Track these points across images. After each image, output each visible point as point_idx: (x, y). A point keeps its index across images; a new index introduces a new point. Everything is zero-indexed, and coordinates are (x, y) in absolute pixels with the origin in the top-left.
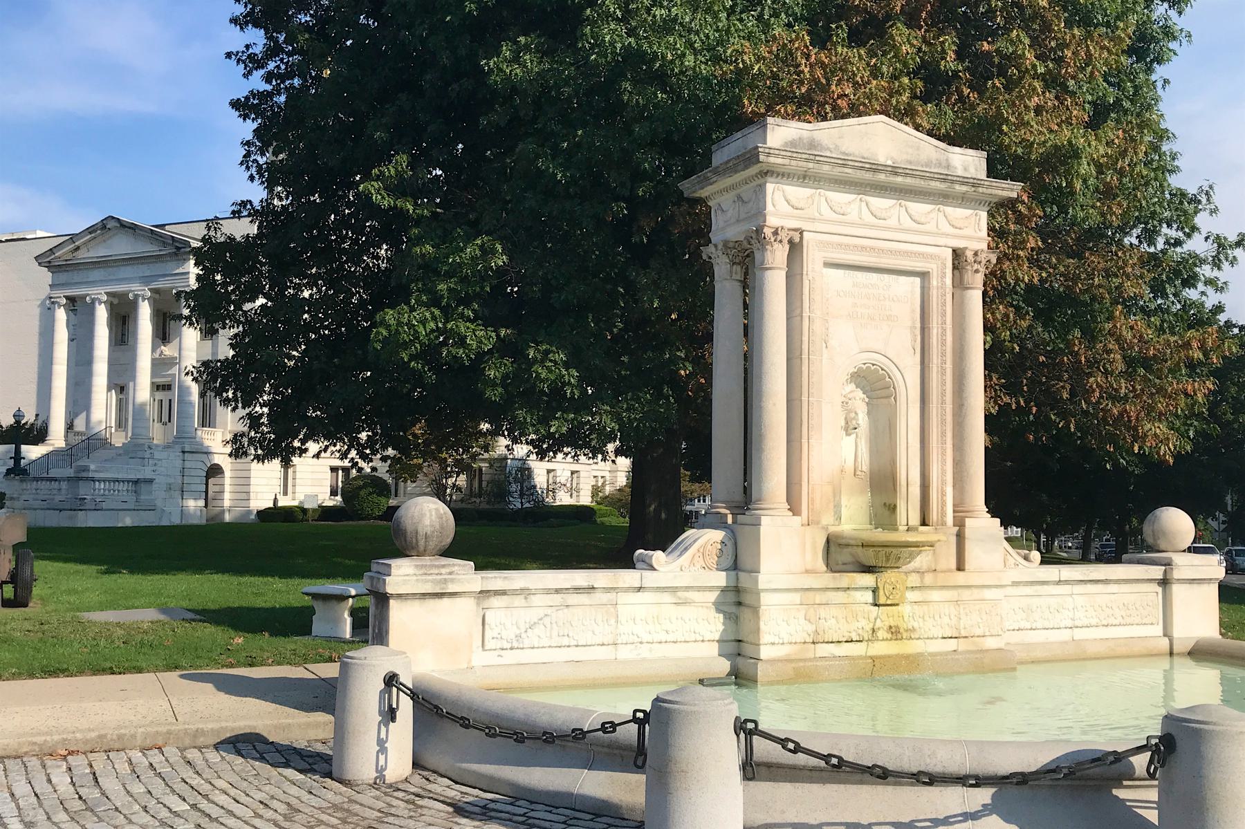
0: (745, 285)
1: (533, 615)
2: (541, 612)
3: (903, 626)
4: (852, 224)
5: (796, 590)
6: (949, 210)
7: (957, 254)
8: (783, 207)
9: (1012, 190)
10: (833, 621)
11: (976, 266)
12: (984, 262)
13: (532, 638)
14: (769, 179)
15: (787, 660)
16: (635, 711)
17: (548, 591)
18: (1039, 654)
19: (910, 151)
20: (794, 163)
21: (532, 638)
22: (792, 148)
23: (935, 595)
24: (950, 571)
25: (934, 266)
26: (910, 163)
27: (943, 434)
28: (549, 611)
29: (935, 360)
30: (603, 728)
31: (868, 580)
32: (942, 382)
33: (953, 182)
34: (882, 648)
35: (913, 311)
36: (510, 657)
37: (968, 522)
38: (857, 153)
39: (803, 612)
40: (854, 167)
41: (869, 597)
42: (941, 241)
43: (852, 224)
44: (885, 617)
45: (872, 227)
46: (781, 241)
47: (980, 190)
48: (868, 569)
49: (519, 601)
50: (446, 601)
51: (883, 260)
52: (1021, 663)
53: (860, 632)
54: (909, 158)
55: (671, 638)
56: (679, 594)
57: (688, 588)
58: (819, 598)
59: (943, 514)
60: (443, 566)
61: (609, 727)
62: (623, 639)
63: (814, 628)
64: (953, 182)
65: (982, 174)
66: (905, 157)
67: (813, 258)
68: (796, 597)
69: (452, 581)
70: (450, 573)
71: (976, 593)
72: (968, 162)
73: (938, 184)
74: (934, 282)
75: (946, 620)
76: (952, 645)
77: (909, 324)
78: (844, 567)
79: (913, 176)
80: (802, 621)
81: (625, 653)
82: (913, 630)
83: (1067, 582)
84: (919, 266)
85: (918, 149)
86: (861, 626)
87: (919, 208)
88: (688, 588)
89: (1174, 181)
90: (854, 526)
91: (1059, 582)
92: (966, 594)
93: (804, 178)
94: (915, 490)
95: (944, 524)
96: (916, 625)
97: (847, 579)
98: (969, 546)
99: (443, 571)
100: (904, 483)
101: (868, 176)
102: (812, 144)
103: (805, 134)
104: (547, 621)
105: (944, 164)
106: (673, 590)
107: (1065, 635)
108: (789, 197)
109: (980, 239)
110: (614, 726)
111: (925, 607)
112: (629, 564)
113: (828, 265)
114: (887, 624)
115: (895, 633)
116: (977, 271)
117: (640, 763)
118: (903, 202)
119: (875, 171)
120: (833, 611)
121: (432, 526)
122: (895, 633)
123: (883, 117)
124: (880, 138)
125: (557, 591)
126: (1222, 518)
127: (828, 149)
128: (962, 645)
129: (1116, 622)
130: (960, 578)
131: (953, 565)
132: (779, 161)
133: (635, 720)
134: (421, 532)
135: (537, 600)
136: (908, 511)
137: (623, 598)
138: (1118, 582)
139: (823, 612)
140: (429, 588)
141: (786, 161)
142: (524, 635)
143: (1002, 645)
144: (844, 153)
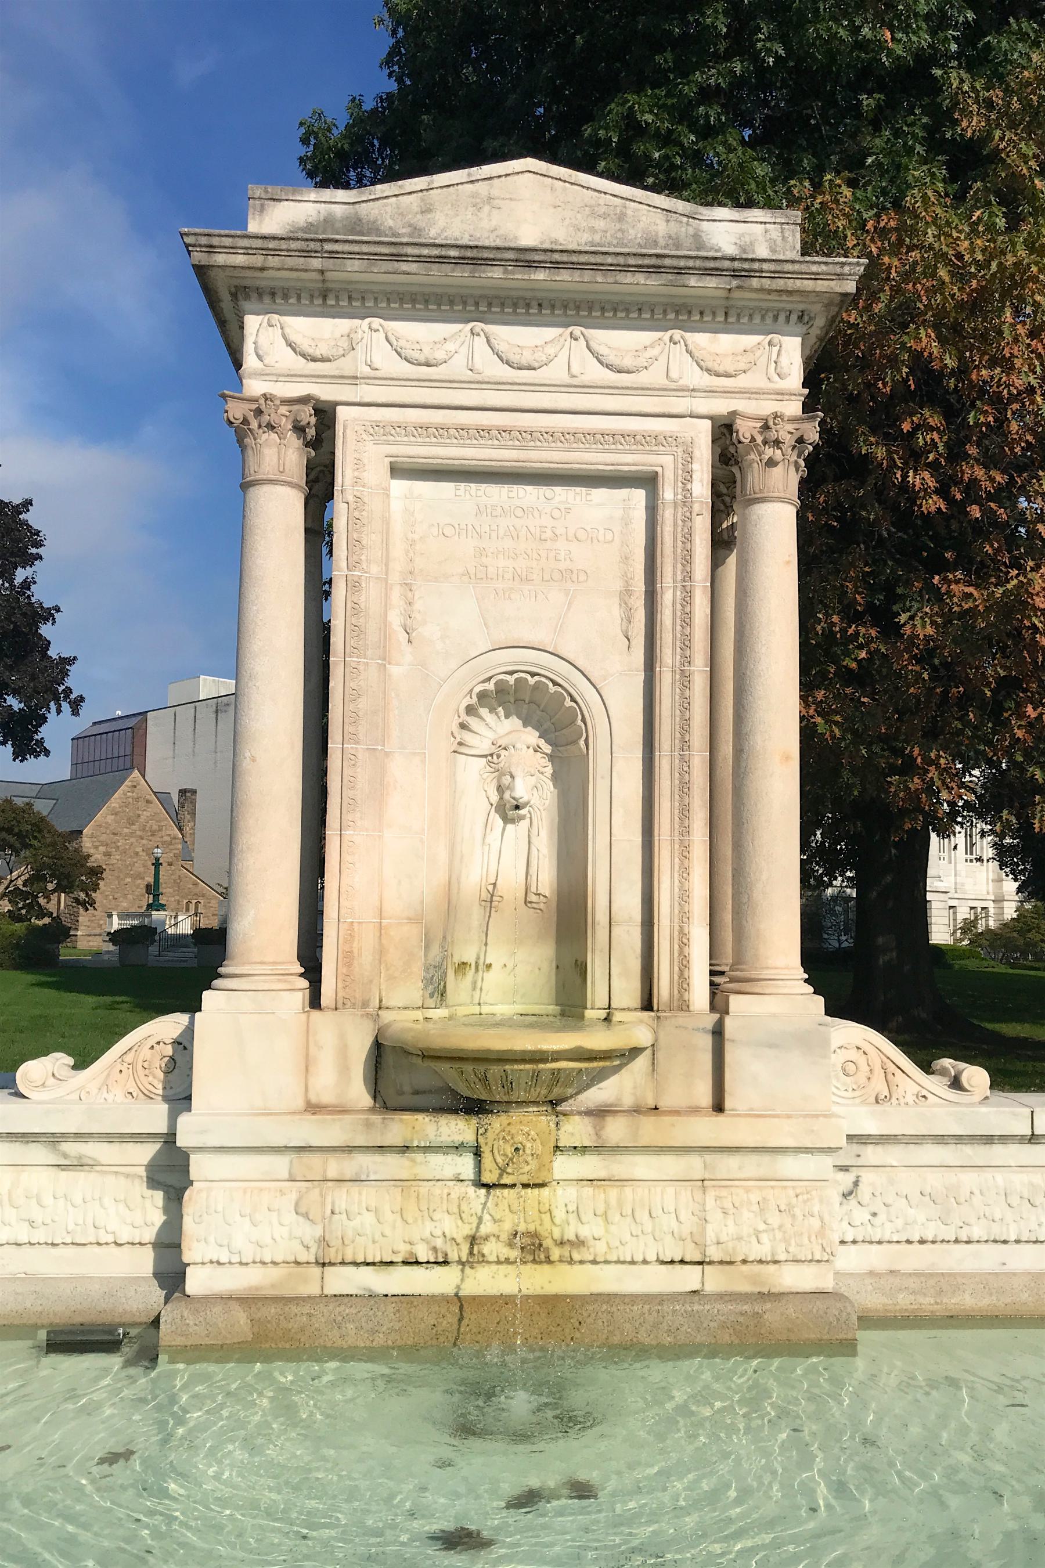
3: (550, 1231)
4: (451, 383)
6: (700, 340)
7: (724, 430)
8: (284, 359)
9: (840, 276)
10: (369, 1218)
11: (769, 452)
12: (789, 440)
14: (246, 305)
15: (247, 1300)
18: (967, 1301)
19: (600, 224)
20: (273, 261)
22: (311, 241)
23: (641, 1166)
24: (694, 1111)
25: (668, 460)
27: (685, 812)
29: (668, 656)
31: (457, 1129)
32: (686, 703)
33: (680, 271)
35: (626, 559)
37: (737, 1003)
39: (294, 1196)
40: (420, 259)
41: (465, 1165)
42: (680, 405)
43: (451, 383)
44: (503, 1214)
45: (498, 385)
46: (271, 427)
47: (755, 283)
48: (474, 1108)
51: (533, 455)
52: (868, 1321)
53: (439, 1243)
55: (40, 1236)
57: (79, 1137)
58: (334, 1166)
59: (682, 982)
63: (318, 1232)
64: (680, 271)
66: (586, 237)
67: (359, 463)
73: (640, 278)
74: (668, 493)
75: (668, 1222)
76: (688, 1279)
77: (618, 585)
78: (418, 1101)
79: (574, 266)
80: (291, 1217)
82: (579, 1243)
84: (629, 461)
85: (621, 217)
86: (448, 1228)
87: (621, 342)
88: (79, 1137)
89: (392, 86)
90: (520, 1008)
92: (730, 1165)
93: (326, 297)
94: (630, 938)
95: (684, 1006)
96: (585, 1232)
97: (402, 1127)
98: (732, 1055)
100: (601, 917)
101: (461, 275)
102: (355, 225)
103: (338, 210)
106: (53, 1139)
108: (293, 337)
109: (781, 395)
111: (613, 1193)
113: (398, 471)
114: (507, 1226)
115: (533, 1249)
116: (771, 463)
118: (577, 330)
119: (477, 262)
120: (368, 1195)
122: (533, 1249)
124: (528, 202)
128: (715, 1281)
130: (707, 1129)
131: (704, 1095)
132: (240, 260)
136: (613, 979)
139: (341, 1197)
141: (258, 260)
143: (828, 1284)
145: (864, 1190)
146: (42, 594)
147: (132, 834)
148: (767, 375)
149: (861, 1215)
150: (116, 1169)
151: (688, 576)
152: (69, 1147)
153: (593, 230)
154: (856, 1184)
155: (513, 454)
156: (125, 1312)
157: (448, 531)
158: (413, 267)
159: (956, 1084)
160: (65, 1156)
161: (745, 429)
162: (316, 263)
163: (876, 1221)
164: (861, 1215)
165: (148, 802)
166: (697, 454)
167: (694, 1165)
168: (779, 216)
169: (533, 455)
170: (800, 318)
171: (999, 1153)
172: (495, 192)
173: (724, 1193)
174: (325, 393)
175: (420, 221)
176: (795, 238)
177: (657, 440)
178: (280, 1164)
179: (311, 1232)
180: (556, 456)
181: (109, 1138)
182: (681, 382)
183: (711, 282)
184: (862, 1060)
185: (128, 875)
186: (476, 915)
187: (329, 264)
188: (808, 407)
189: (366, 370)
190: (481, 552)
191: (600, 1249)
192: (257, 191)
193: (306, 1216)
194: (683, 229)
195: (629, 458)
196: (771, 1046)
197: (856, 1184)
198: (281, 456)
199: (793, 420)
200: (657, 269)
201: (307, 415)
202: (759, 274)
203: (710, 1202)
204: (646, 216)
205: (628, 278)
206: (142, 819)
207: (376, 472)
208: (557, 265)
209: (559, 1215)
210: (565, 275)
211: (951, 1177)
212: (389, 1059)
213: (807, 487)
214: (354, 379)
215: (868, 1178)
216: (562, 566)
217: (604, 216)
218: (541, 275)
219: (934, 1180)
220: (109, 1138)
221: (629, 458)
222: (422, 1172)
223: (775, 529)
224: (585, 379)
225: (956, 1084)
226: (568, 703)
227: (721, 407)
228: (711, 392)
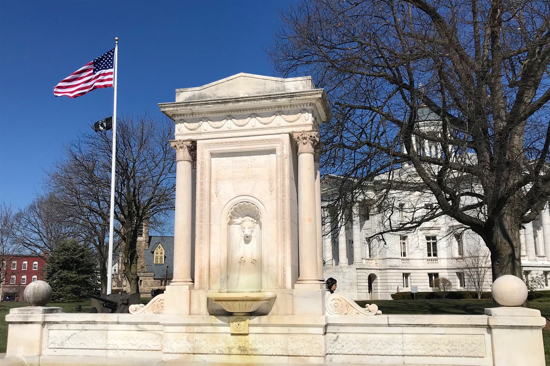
5: (31, 323)
7: (291, 136)
11: (305, 141)
19: (259, 87)
20: (179, 108)
21: (68, 344)
26: (260, 93)
28: (76, 332)
36: (59, 352)
38: (226, 95)
40: (212, 104)
42: (280, 131)
47: (295, 98)
49: (64, 326)
53: (221, 349)
54: (258, 91)
56: (139, 326)
57: (143, 323)
58: (196, 329)
60: (29, 310)
62: (111, 347)
66: (255, 91)
67: (202, 153)
69: (30, 316)
70: (32, 313)
71: (301, 330)
73: (266, 101)
81: (111, 354)
84: (268, 146)
88: (143, 323)
92: (294, 330)
96: (257, 347)
99: (29, 312)
103: (197, 92)
106: (136, 324)
109: (306, 125)
112: (481, 312)
113: (213, 155)
114: (238, 345)
123: (242, 74)
124: (243, 85)
125: (80, 323)
126: (35, 277)
127: (210, 97)
129: (444, 354)
134: (26, 296)
137: (111, 327)
138: (442, 326)
142: (64, 342)
144: (219, 97)
145: (340, 340)
149: (339, 346)
151: (283, 174)
152: (141, 326)
153: (257, 89)
154: (338, 337)
156: (43, 293)
157: (225, 168)
158: (211, 106)
160: (139, 328)
161: (295, 136)
162: (189, 107)
163: (343, 348)
164: (339, 346)
166: (285, 143)
168: (305, 78)
170: (310, 105)
171: (378, 330)
173: (293, 337)
175: (215, 92)
177: (275, 140)
178: (183, 329)
179: (190, 345)
182: (280, 125)
183: (284, 100)
184: (339, 303)
187: (191, 107)
189: (203, 131)
191: (261, 352)
192: (177, 90)
193: (189, 341)
194: (278, 85)
195: (268, 145)
197: (338, 337)
198: (182, 154)
200: (270, 98)
201: (189, 143)
202: (296, 96)
204: (268, 84)
205: (263, 101)
207: (207, 156)
208: (245, 101)
209: (250, 342)
210: (247, 103)
212: (210, 302)
215: (341, 335)
218: (241, 103)
221: (268, 145)
226: (257, 209)
227: (290, 130)
228: (288, 127)
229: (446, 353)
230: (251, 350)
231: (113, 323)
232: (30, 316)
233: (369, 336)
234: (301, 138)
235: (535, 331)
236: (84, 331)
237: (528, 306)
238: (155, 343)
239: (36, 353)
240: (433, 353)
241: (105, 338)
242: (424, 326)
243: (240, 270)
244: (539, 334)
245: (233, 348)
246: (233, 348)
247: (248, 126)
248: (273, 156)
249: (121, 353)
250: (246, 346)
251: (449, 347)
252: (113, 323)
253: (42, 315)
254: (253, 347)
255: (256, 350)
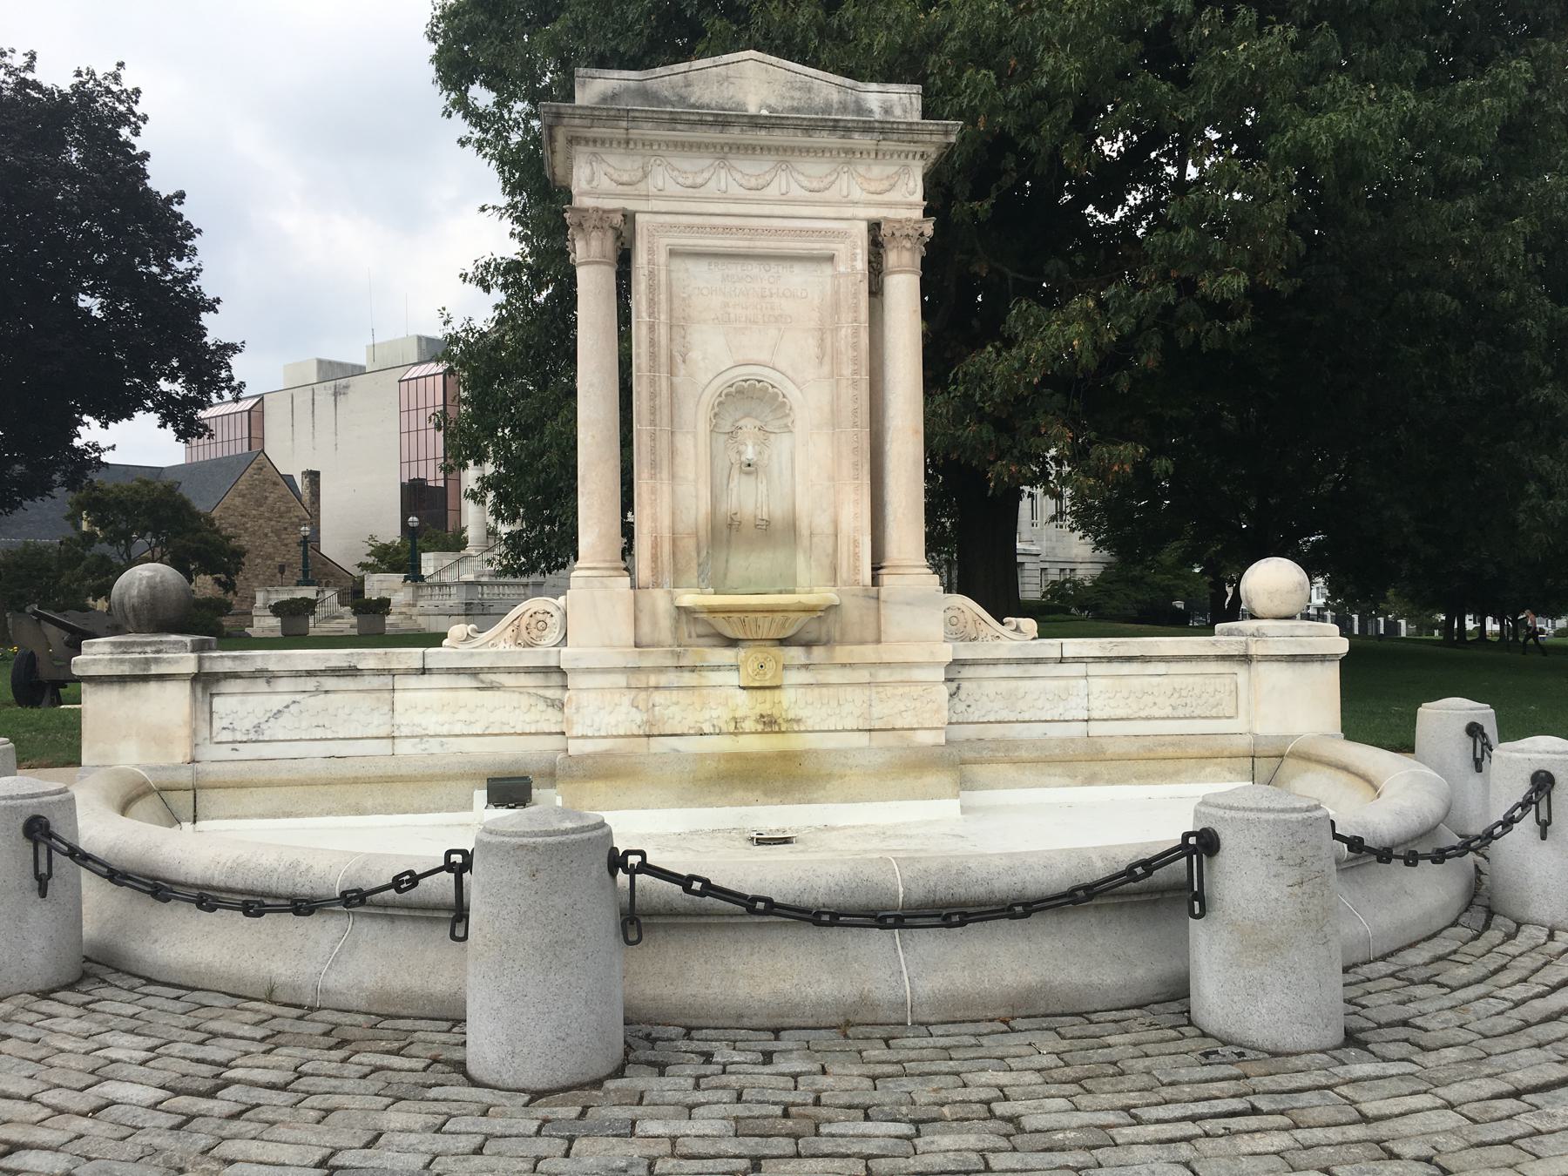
0: (150, 981)
1: (277, 702)
2: (288, 698)
5: (161, 678)
7: (874, 227)
13: (276, 729)
16: (449, 853)
17: (297, 674)
19: (797, 94)
28: (298, 697)
30: (396, 883)
34: (754, 744)
36: (247, 751)
42: (848, 212)
49: (261, 685)
50: (153, 687)
60: (149, 644)
61: (406, 881)
62: (405, 731)
65: (916, 117)
66: (788, 103)
68: (621, 680)
69: (156, 660)
71: (898, 675)
72: (897, 100)
83: (1078, 660)
84: (818, 246)
85: (809, 90)
88: (492, 670)
91: (1062, 660)
92: (883, 675)
96: (801, 714)
104: (293, 708)
105: (852, 106)
106: (474, 673)
107: (1078, 729)
109: (910, 206)
110: (414, 879)
113: (673, 253)
117: (460, 933)
121: (139, 596)
122: (769, 723)
123: (752, 53)
124: (753, 80)
129: (1162, 713)
133: (448, 866)
135: (283, 685)
139: (658, 697)
140: (125, 670)
145: (962, 694)
146: (207, 285)
147: (261, 515)
148: (899, 193)
150: (519, 689)
153: (792, 98)
155: (746, 243)
159: (1017, 629)
161: (885, 230)
165: (275, 484)
167: (863, 675)
169: (758, 244)
172: (731, 73)
174: (631, 205)
176: (917, 102)
179: (639, 717)
180: (772, 244)
181: (510, 671)
185: (258, 556)
186: (725, 532)
188: (927, 213)
190: (726, 305)
191: (809, 725)
196: (908, 604)
199: (916, 222)
203: (874, 696)
204: (827, 87)
206: (270, 500)
209: (785, 705)
211: (1013, 683)
213: (927, 265)
214: (647, 197)
215: (965, 685)
216: (777, 313)
217: (800, 89)
219: (1004, 686)
220: (510, 671)
221: (799, 245)
222: (704, 682)
223: (904, 291)
224: (791, 195)
225: (1017, 629)
227: (875, 213)
228: (868, 204)
229: (1168, 711)
230: (788, 721)
231: (408, 672)
232: (156, 660)
233: (1021, 683)
234: (897, 234)
235: (1316, 668)
236: (322, 696)
237: (674, 612)
238: (528, 718)
239: (180, 753)
240: (1143, 714)
241: (387, 708)
242: (1130, 659)
243: (729, 541)
244: (1332, 673)
245: (744, 719)
246: (744, 719)
247: (772, 191)
248: (827, 269)
249: (433, 746)
250: (776, 713)
251: (1173, 701)
252: (408, 672)
253: (193, 655)
254: (791, 715)
255: (798, 721)
